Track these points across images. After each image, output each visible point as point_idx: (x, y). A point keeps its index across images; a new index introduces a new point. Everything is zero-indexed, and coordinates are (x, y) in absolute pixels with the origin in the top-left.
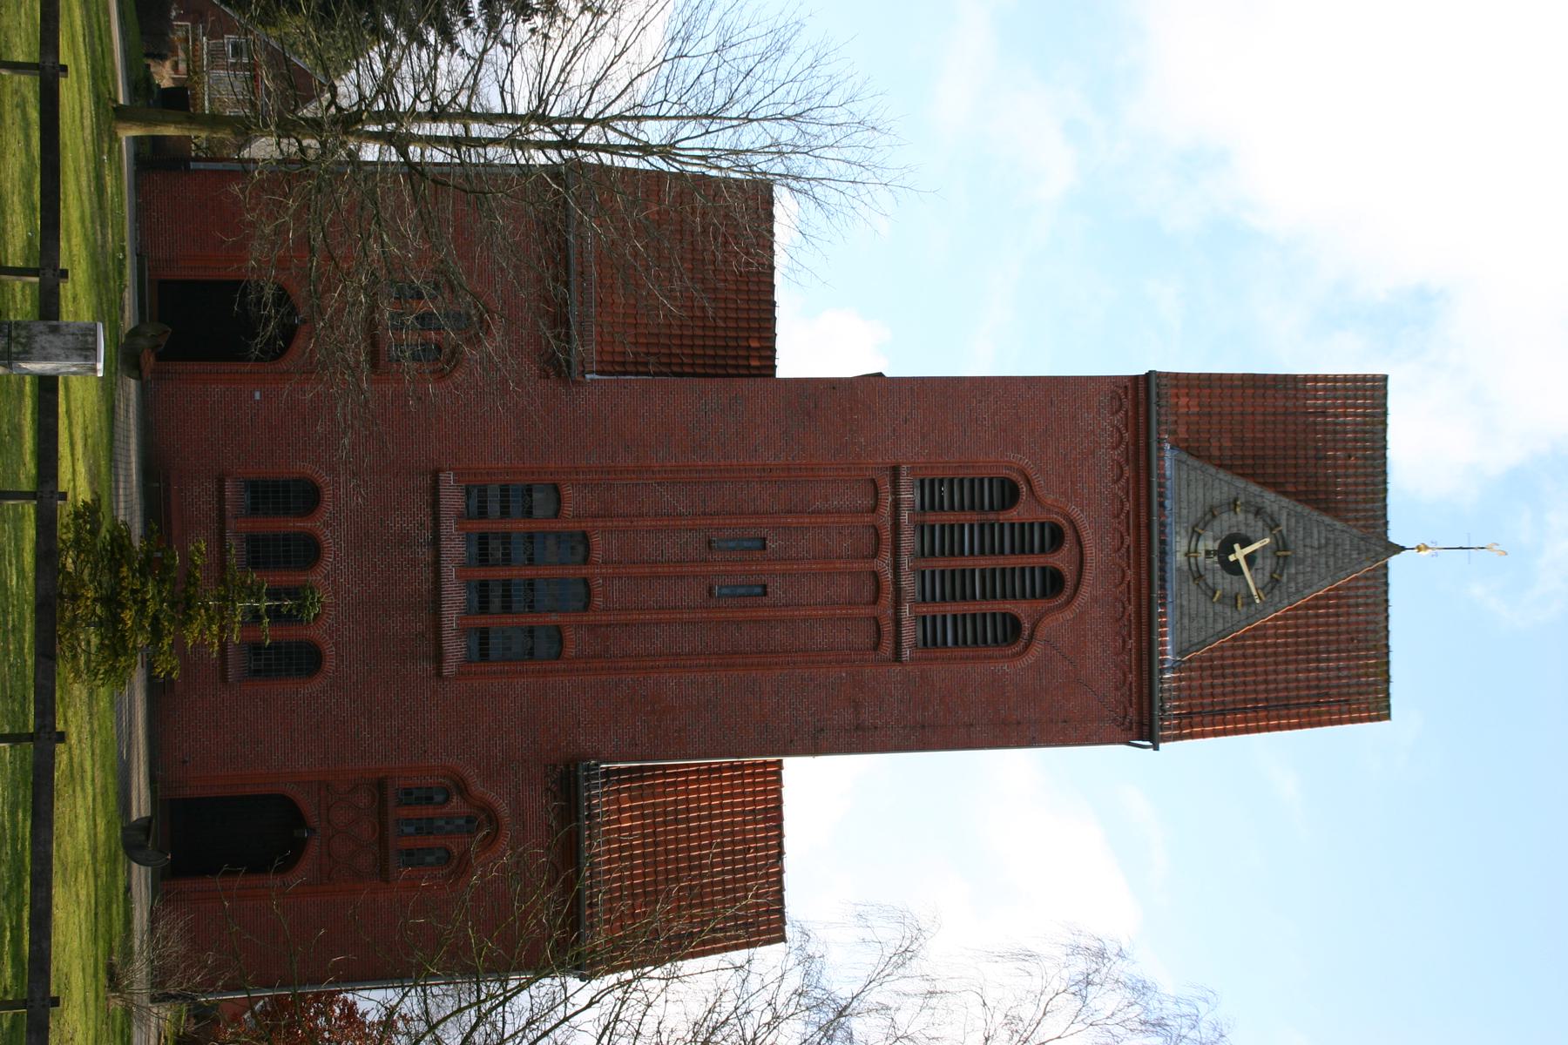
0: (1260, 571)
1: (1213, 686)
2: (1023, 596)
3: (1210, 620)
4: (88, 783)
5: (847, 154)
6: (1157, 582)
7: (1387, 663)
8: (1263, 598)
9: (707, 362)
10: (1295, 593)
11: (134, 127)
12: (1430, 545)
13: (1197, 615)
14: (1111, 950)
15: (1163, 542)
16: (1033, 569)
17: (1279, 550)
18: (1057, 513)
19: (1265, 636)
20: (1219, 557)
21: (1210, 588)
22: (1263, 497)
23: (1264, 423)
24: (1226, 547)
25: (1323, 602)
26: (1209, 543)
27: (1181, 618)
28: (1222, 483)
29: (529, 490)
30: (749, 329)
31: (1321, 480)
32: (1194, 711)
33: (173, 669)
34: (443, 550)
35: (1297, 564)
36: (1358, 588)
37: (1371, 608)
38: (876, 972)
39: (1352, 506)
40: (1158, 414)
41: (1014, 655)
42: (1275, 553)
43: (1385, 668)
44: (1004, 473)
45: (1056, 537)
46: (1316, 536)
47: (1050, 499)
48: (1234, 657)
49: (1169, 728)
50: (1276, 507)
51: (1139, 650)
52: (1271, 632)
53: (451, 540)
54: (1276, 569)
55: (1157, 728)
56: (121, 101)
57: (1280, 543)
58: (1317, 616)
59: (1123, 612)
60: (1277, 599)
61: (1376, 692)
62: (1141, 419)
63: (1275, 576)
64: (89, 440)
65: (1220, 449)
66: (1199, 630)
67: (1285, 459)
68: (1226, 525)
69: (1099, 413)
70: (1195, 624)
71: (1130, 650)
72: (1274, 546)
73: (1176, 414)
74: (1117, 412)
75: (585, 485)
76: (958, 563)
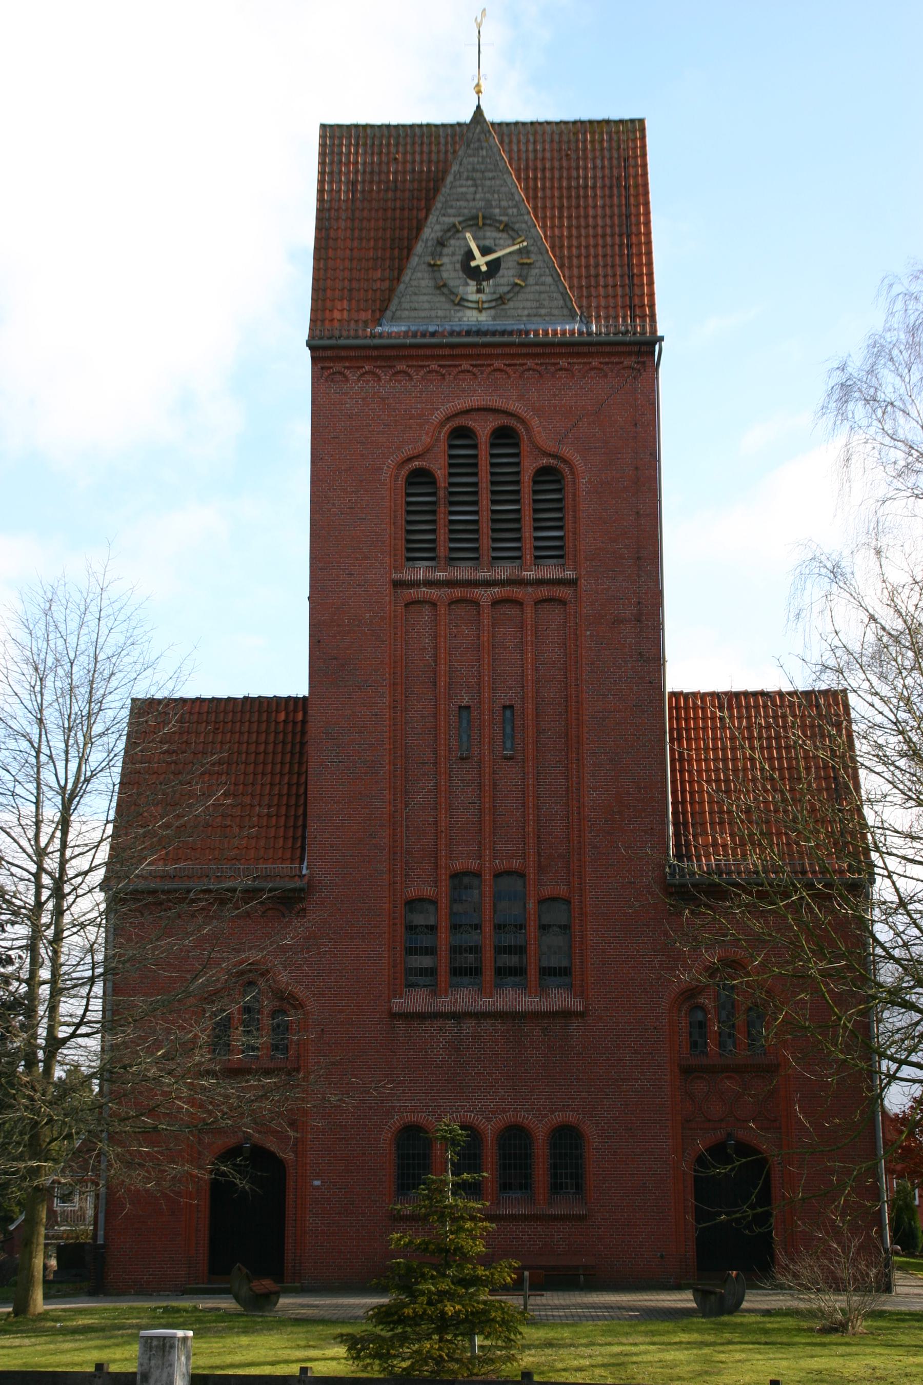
0: (497, 242)
1: (606, 286)
2: (517, 464)
3: (543, 288)
4: (634, 1349)
5: (73, 625)
6: (506, 339)
7: (591, 122)
8: (523, 238)
9: (297, 760)
10: (519, 209)
11: (34, 1297)
12: (476, 82)
13: (537, 301)
14: (839, 377)
15: (468, 333)
16: (492, 456)
17: (478, 224)
18: (440, 433)
19: (561, 237)
20: (484, 280)
21: (512, 289)
22: (427, 240)
23: (361, 239)
24: (474, 273)
25: (531, 183)
26: (470, 290)
27: (540, 316)
28: (413, 277)
29: (411, 928)
30: (268, 721)
31: (416, 185)
32: (628, 303)
33: (510, 1266)
34: (465, 1009)
35: (491, 207)
36: (519, 151)
37: (539, 138)
38: (852, 600)
39: (442, 156)
40: (348, 338)
41: (573, 473)
42: (480, 228)
43: (596, 124)
44: (401, 482)
45: (462, 434)
46: (464, 190)
47: (426, 439)
48: (579, 267)
49: (643, 327)
50: (437, 227)
51: (571, 355)
52: (557, 231)
53: (456, 1002)
54: (495, 227)
55: (643, 338)
56: (11, 1309)
57: (471, 223)
58: (544, 188)
59: (534, 370)
60: (524, 226)
61: (618, 132)
62: (352, 353)
63: (501, 227)
64: (311, 1343)
65: (382, 280)
66: (551, 299)
67: (395, 219)
68: (453, 274)
69: (346, 394)
70: (546, 303)
71: (569, 363)
72: (474, 228)
73: (349, 321)
74: (345, 376)
75: (407, 875)
76: (485, 525)
